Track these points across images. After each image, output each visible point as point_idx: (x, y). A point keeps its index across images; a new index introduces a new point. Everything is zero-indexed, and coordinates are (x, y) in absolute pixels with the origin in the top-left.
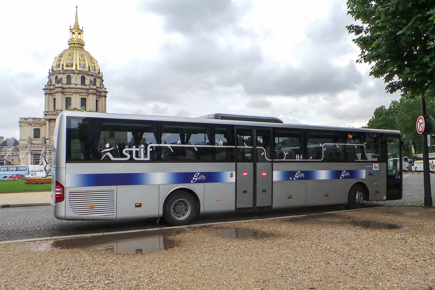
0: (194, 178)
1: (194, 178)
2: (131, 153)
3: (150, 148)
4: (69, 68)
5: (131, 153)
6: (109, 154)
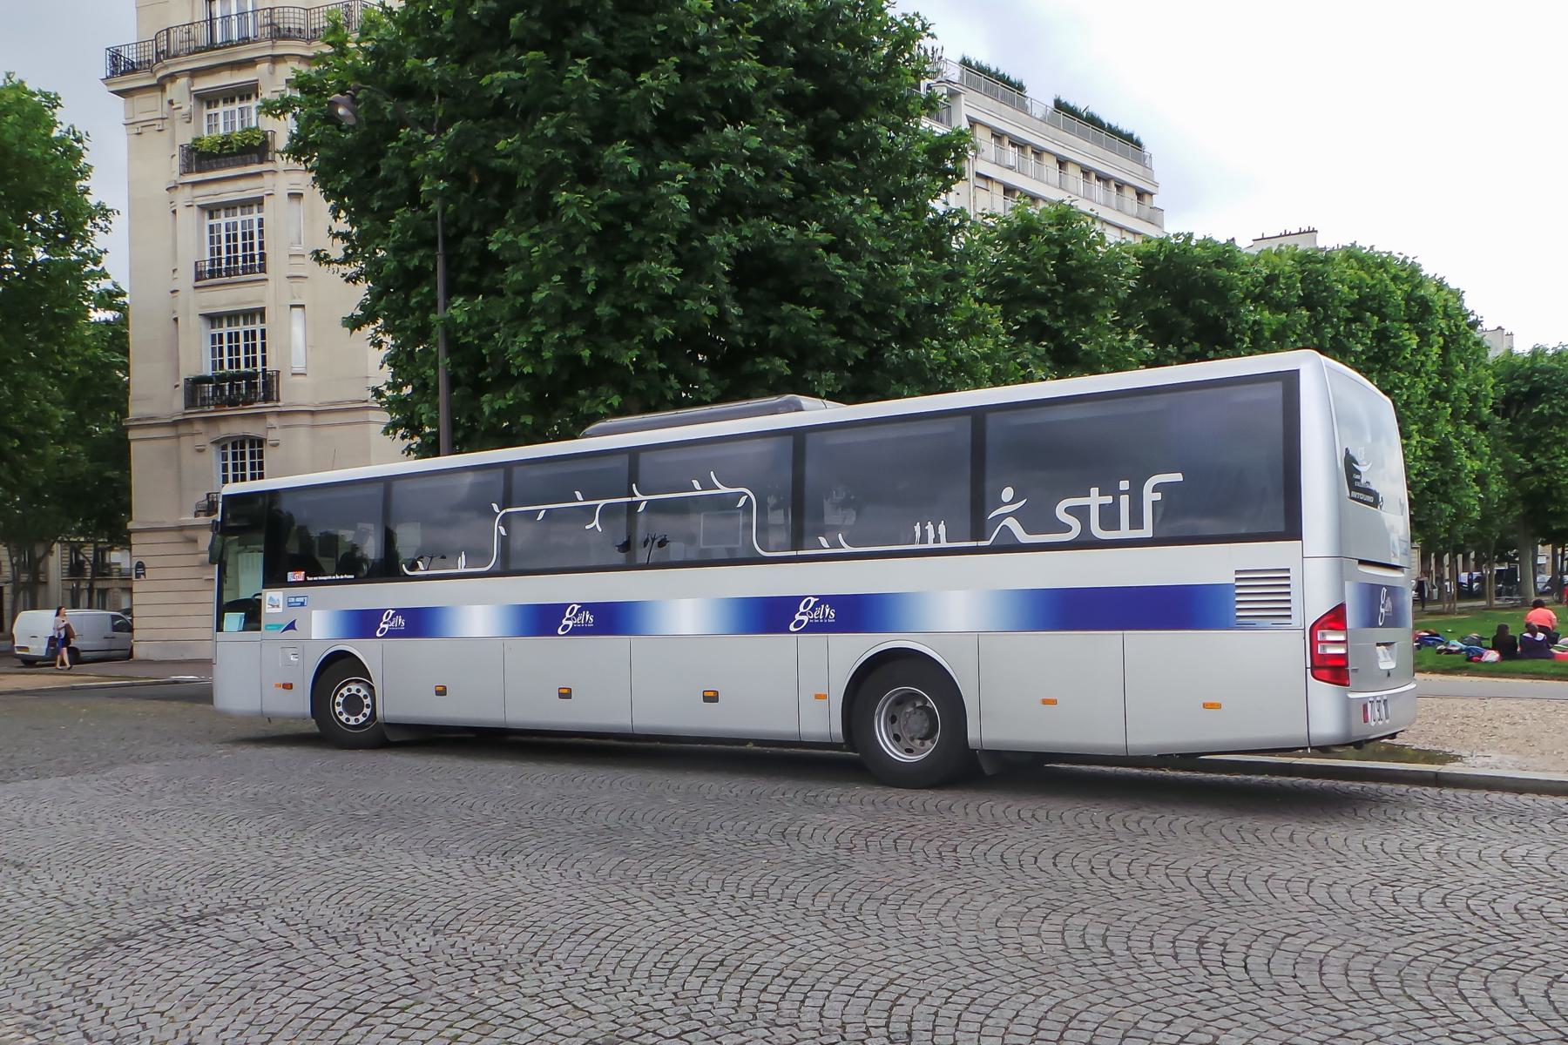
0: (798, 617)
1: (798, 617)
2: (1081, 513)
3: (1155, 490)
5: (1081, 513)
6: (1012, 523)
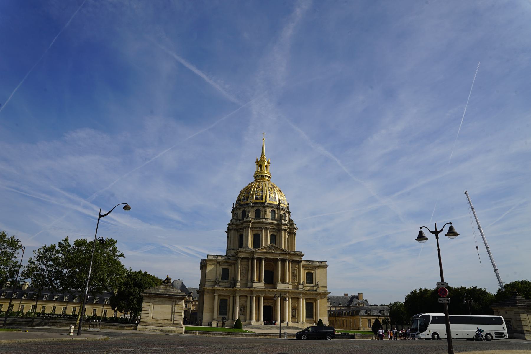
4: (258, 201)
